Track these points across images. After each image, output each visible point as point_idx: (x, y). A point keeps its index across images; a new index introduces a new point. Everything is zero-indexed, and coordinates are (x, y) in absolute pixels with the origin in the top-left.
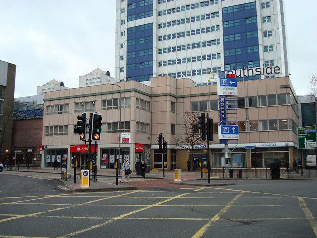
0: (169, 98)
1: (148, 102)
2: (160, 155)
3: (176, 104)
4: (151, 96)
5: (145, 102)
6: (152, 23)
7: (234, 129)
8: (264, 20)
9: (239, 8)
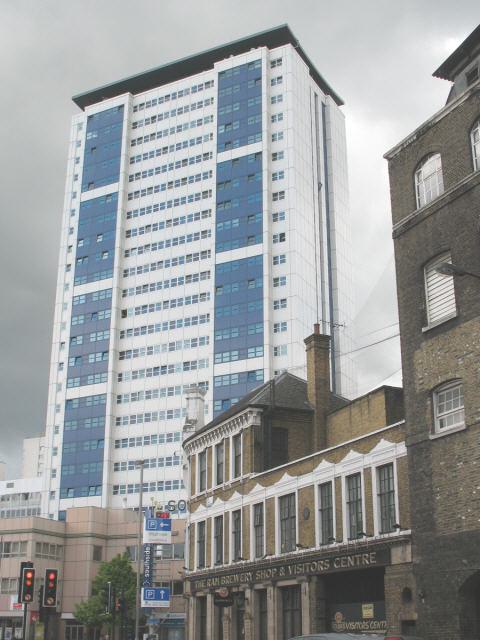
0: (89, 540)
1: (59, 546)
2: (74, 629)
3: (104, 549)
4: (65, 537)
5: (53, 546)
6: (262, 255)
7: (162, 592)
8: (276, 305)
9: (239, 378)
